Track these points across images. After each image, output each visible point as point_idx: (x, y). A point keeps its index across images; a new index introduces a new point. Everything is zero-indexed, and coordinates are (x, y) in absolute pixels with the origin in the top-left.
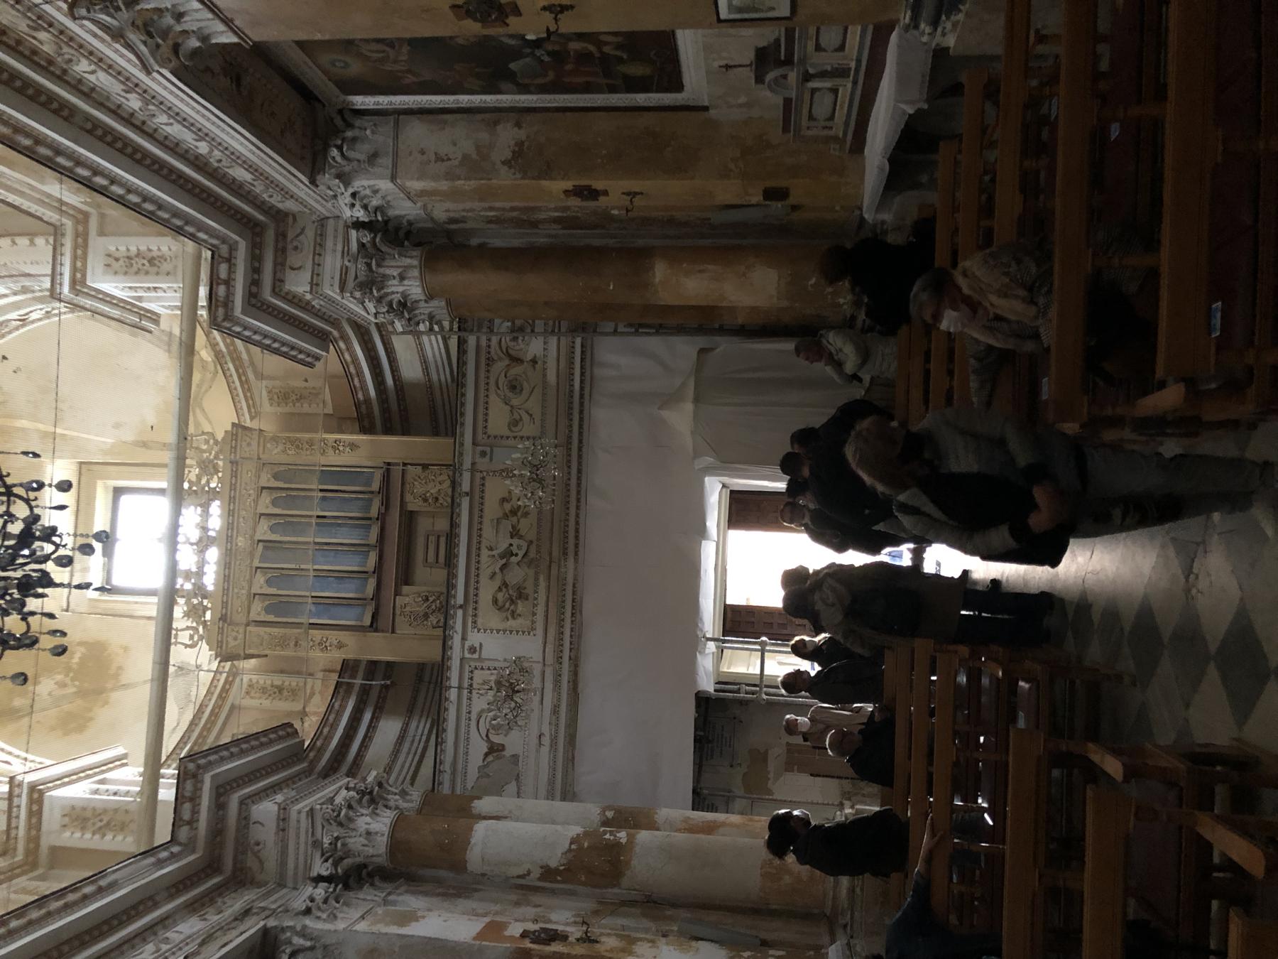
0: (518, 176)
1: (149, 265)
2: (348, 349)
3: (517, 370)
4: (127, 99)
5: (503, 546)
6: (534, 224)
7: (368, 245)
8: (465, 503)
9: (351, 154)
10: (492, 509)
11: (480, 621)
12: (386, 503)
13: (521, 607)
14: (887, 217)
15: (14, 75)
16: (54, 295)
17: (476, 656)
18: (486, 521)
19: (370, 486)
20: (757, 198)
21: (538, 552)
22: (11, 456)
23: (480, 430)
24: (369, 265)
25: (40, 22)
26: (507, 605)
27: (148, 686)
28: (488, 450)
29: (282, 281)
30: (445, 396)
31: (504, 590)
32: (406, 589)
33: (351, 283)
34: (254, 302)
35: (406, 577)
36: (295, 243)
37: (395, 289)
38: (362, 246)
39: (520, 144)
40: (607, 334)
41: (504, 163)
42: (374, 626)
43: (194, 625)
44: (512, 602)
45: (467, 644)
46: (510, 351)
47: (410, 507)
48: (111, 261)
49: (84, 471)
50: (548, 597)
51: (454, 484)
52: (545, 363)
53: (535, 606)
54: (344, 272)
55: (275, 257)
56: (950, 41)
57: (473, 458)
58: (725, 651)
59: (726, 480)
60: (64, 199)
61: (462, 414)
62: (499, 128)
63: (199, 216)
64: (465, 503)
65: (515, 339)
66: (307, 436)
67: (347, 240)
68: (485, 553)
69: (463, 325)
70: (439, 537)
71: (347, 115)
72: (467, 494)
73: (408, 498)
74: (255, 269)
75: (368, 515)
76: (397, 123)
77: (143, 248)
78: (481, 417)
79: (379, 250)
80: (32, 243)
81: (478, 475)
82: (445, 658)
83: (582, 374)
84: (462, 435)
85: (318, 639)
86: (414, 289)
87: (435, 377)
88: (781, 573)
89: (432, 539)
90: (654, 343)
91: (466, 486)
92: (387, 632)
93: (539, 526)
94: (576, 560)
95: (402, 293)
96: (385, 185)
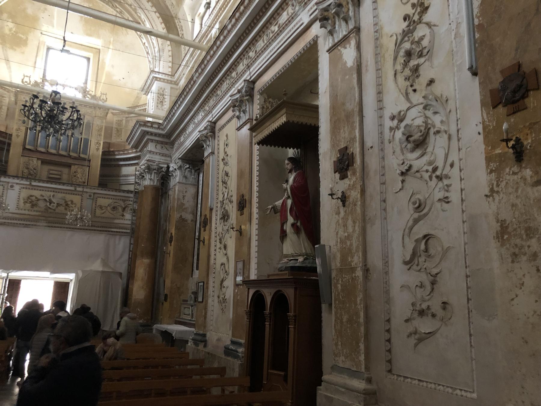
0: (177, 220)
1: (160, 101)
2: (133, 152)
3: (120, 209)
4: (253, 52)
5: (54, 200)
6: (166, 221)
7: (162, 170)
8: (73, 188)
9: (187, 171)
10: (69, 197)
11: (24, 190)
12: (75, 158)
13: (28, 205)
14: (154, 331)
15: (270, 6)
16: (152, 71)
17: (9, 187)
18: (63, 195)
19: (82, 154)
20: (166, 292)
21: (50, 212)
22: (98, 54)
23: (98, 195)
24: (155, 169)
25: (304, 3)
26: (30, 200)
27: (9, 81)
28: (92, 198)
29: (152, 142)
30: (116, 181)
31: (36, 199)
32: (40, 162)
33: (150, 163)
34: (145, 133)
35: (44, 162)
36: (164, 147)
37: (147, 176)
38: (162, 168)
39: (186, 221)
40: (130, 241)
41: (181, 216)
42: (24, 149)
43: (31, 84)
44: (30, 202)
45: (15, 185)
46: (127, 208)
47: (73, 167)
48: (163, 89)
49: (97, 50)
50: (31, 215)
51: (79, 185)
52: (122, 219)
53: (28, 210)
54: (154, 162)
55: (160, 141)
56: (189, 344)
57: (89, 192)
58: (2, 280)
59: (73, 281)
60: (214, 29)
61: (105, 190)
62: (191, 215)
63: (171, 124)
64: (73, 188)
65: (131, 210)
66: (103, 134)
67: (164, 163)
68: (52, 194)
69: (136, 193)
70: (60, 175)
71: (198, 171)
72: (76, 189)
73: (76, 166)
74: (156, 135)
75: (71, 151)
76: (194, 185)
77: (166, 100)
78: (104, 196)
79: (160, 173)
80: (170, 67)
81: (81, 193)
82: (9, 176)
83: (117, 232)
84: (98, 189)
85: (21, 128)
86: (147, 182)
87: (122, 178)
88: (30, 300)
89: (60, 173)
90: (126, 257)
91: (78, 189)
92: (22, 153)
93: (61, 213)
94: (46, 226)
95: (146, 179)
96: (177, 179)
